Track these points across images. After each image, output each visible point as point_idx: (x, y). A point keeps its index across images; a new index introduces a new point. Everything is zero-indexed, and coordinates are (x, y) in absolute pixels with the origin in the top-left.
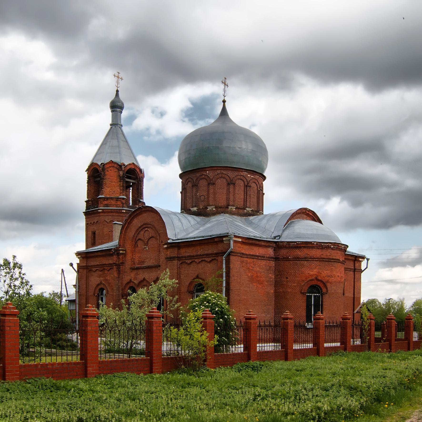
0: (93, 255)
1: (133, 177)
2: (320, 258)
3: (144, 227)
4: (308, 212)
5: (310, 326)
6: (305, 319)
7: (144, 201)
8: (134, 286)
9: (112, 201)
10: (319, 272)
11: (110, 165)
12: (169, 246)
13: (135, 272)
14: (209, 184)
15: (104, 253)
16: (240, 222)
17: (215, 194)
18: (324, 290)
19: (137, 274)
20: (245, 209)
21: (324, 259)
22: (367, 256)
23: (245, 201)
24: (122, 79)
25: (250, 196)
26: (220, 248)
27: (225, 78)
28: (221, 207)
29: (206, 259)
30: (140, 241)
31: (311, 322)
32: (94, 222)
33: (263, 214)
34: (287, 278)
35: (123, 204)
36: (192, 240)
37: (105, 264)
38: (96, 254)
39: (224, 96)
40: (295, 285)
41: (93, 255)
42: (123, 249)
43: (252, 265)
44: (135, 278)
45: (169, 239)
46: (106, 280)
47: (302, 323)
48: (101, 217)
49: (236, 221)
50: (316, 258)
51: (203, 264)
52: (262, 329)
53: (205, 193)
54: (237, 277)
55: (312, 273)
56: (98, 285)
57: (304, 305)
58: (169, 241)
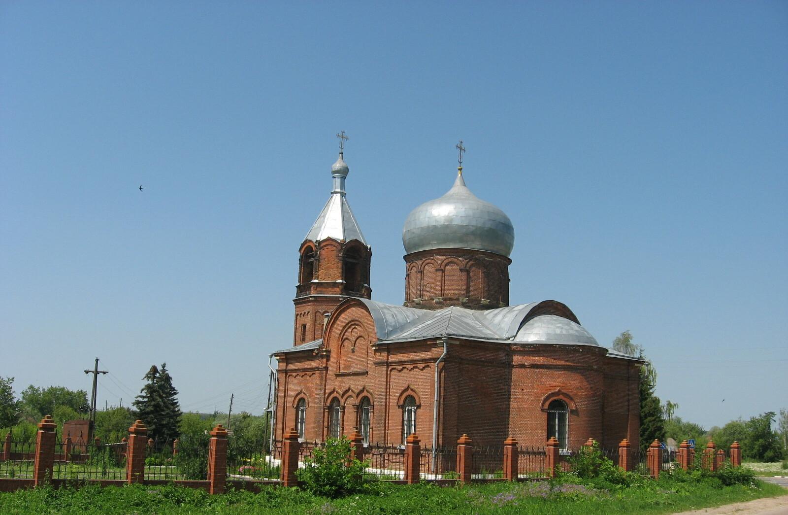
8: (337, 395)
13: (340, 379)
24: (347, 139)
32: (305, 313)
34: (523, 390)
37: (307, 369)
38: (297, 355)
39: (460, 163)
44: (340, 387)
46: (307, 388)
56: (299, 394)
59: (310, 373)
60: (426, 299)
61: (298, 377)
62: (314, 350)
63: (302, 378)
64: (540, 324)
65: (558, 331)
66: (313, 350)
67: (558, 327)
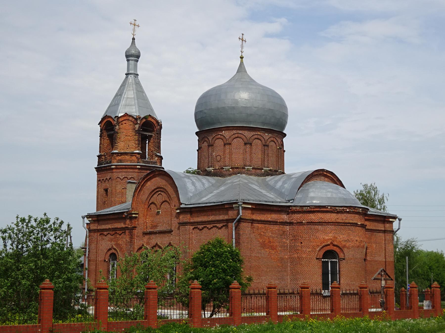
0: (105, 218)
1: (149, 129)
2: (335, 223)
3: (158, 190)
4: (325, 173)
5: (326, 293)
6: (321, 286)
7: (161, 155)
9: (126, 156)
10: (334, 237)
11: (125, 118)
12: (182, 210)
13: (147, 237)
14: (225, 145)
15: (116, 217)
16: (256, 183)
17: (231, 154)
18: (341, 256)
19: (149, 238)
20: (263, 169)
21: (340, 223)
22: (399, 216)
23: (263, 161)
25: (268, 155)
26: (231, 214)
27: (243, 34)
28: (237, 168)
29: (218, 225)
30: (152, 205)
31: (328, 289)
32: (107, 179)
33: (284, 173)
34: (301, 243)
35: (138, 159)
36: (204, 205)
37: (117, 228)
38: (108, 217)
40: (310, 250)
41: (105, 218)
42: (135, 212)
43: (263, 230)
45: (181, 204)
47: (319, 291)
48: (114, 173)
49: (252, 183)
50: (331, 223)
51: (214, 229)
52: (291, 296)
53: (221, 154)
54: (248, 243)
55: (327, 238)
56: (110, 249)
57: (319, 272)
58: (182, 206)
59: (121, 232)
60: (217, 168)
61: (109, 236)
62: (124, 212)
63: (112, 237)
64: (314, 190)
65: (329, 195)
66: (123, 213)
67: (329, 192)
